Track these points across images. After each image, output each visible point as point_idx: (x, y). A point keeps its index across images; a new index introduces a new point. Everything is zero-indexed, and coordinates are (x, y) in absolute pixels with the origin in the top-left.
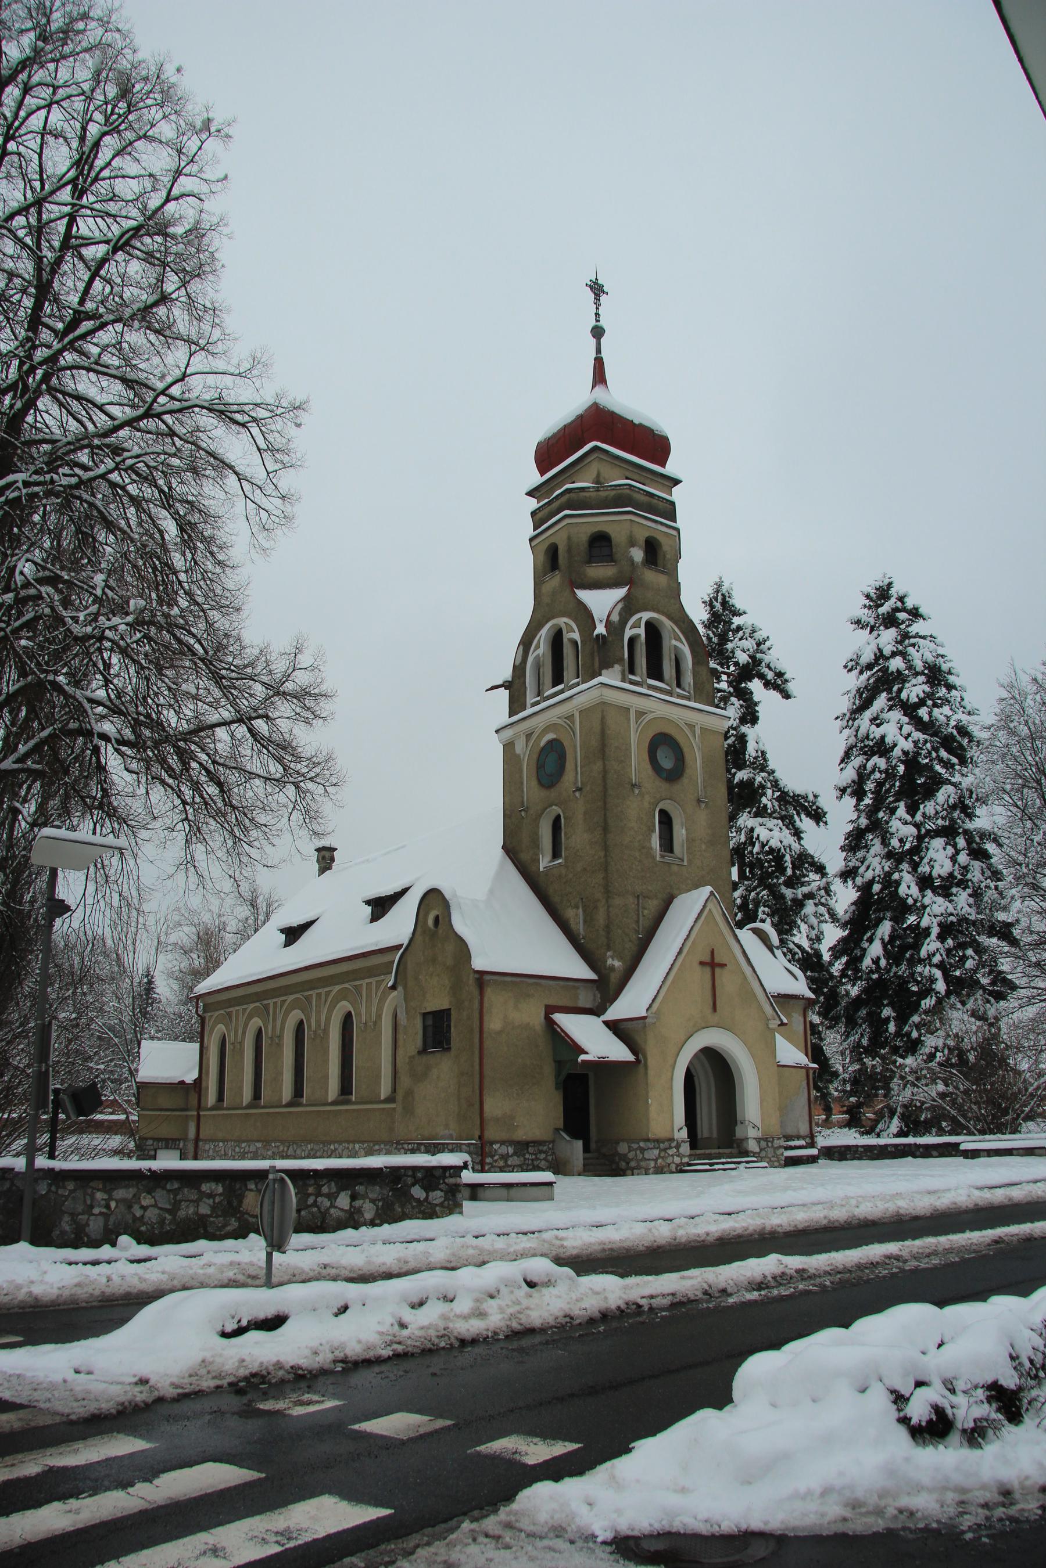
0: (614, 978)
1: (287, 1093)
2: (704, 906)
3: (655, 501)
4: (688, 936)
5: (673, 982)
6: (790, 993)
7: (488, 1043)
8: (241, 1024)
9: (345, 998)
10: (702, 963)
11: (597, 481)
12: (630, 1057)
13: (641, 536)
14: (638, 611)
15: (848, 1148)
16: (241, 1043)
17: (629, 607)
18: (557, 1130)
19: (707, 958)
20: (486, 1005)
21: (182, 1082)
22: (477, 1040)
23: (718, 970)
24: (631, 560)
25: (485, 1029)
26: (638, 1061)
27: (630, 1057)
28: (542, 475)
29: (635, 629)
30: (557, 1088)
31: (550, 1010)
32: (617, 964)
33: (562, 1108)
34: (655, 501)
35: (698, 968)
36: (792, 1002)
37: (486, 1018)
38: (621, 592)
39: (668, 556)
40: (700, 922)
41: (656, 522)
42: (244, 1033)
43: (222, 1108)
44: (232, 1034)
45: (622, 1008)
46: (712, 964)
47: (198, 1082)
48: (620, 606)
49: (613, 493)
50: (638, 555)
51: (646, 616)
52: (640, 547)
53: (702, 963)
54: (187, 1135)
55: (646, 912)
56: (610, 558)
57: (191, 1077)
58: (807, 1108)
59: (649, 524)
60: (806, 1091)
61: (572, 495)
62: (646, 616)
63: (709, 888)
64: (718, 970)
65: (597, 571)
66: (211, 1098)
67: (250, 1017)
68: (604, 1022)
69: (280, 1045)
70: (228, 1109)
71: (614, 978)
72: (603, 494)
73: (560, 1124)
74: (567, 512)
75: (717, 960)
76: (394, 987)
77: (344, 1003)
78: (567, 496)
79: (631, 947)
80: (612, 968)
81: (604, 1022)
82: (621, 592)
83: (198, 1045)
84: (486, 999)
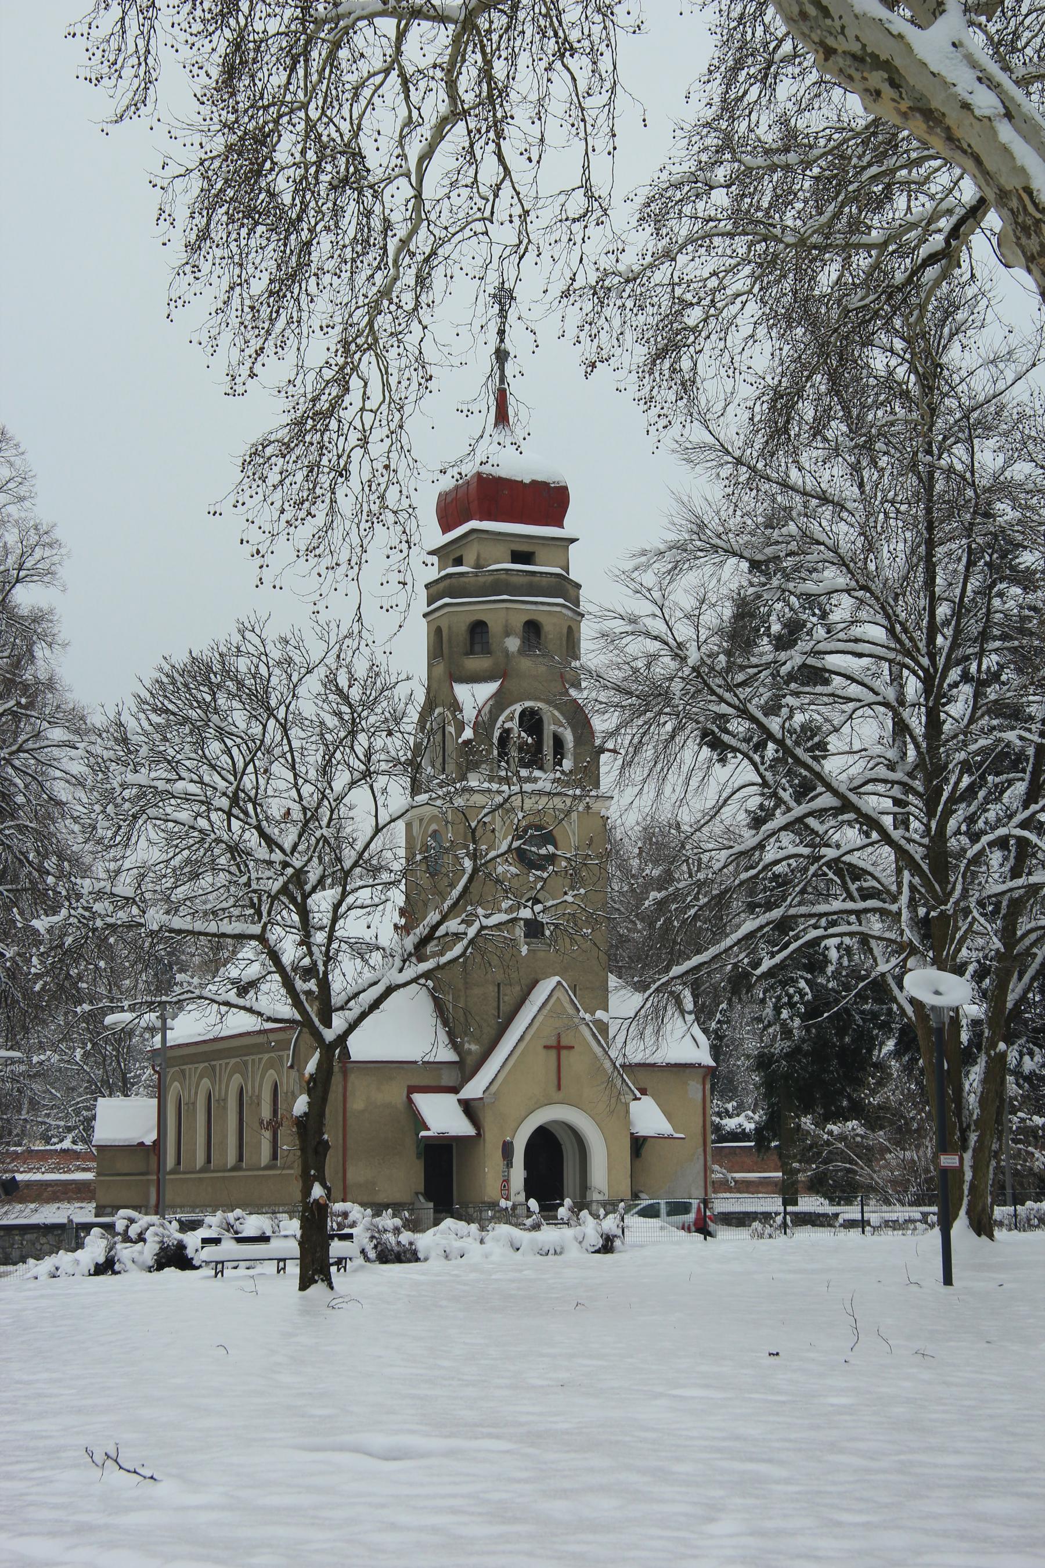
0: (470, 1061)
1: (231, 1159)
2: (550, 996)
3: (536, 579)
4: (530, 1025)
5: (514, 1066)
6: (683, 1061)
7: (350, 1121)
8: (194, 1080)
9: (272, 1067)
10: (546, 1047)
11: (478, 566)
12: (470, 1131)
13: (518, 622)
14: (511, 704)
15: (819, 1215)
16: (194, 1104)
17: (500, 701)
18: (417, 1194)
19: (553, 1042)
20: (349, 1088)
21: (142, 1144)
22: (341, 1118)
23: (564, 1053)
24: (506, 652)
25: (348, 1109)
26: (479, 1135)
27: (470, 1131)
28: (446, 528)
29: (509, 719)
30: (418, 1158)
31: (413, 1089)
32: (474, 1047)
33: (423, 1175)
34: (536, 579)
35: (544, 1052)
36: (688, 1071)
37: (349, 1100)
38: (492, 687)
39: (550, 636)
40: (545, 1012)
41: (536, 603)
42: (196, 1093)
43: (179, 1173)
44: (186, 1093)
45: (474, 1089)
46: (558, 1048)
47: (158, 1145)
48: (491, 703)
49: (491, 578)
50: (513, 644)
51: (518, 708)
52: (516, 635)
53: (546, 1047)
54: (148, 1201)
55: (506, 998)
56: (487, 650)
57: (150, 1138)
58: (702, 1174)
59: (529, 607)
60: (702, 1158)
61: (453, 580)
62: (518, 708)
63: (557, 978)
64: (564, 1053)
65: (475, 663)
66: (170, 1162)
67: (201, 1077)
68: (459, 1101)
69: (225, 1108)
70: (185, 1173)
71: (470, 1061)
72: (481, 579)
73: (422, 1189)
74: (447, 600)
75: (555, 1044)
76: (292, 1067)
77: (272, 1071)
78: (448, 581)
79: (489, 1032)
80: (469, 1051)
81: (459, 1101)
82: (492, 687)
83: (155, 1101)
84: (349, 1085)
